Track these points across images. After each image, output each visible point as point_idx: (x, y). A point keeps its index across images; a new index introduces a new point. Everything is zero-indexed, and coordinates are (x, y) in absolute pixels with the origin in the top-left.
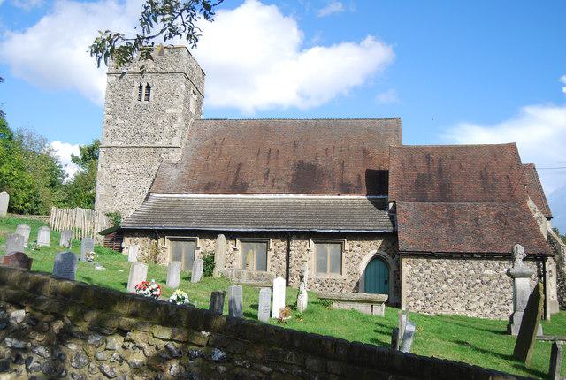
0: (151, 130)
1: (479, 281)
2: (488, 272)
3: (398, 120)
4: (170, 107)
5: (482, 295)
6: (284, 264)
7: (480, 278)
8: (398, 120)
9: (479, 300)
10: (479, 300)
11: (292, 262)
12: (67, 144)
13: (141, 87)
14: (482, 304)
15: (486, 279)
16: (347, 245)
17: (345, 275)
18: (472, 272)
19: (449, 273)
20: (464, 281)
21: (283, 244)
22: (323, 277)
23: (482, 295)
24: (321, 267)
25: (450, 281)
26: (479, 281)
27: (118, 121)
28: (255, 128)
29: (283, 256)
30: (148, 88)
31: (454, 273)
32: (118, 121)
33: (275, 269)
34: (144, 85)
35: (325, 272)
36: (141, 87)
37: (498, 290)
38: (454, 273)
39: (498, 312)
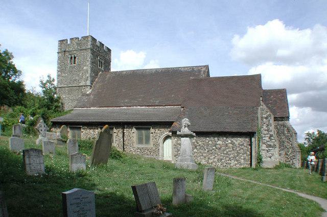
0: (77, 78)
1: (214, 148)
2: (219, 142)
3: (207, 67)
4: (85, 66)
5: (216, 155)
6: (122, 139)
7: (215, 146)
8: (207, 67)
9: (214, 158)
10: (214, 158)
11: (125, 139)
12: (128, 51)
13: (72, 58)
14: (216, 160)
15: (218, 146)
16: (152, 130)
17: (152, 146)
18: (210, 142)
19: (198, 143)
20: (205, 147)
21: (121, 130)
22: (140, 146)
23: (216, 155)
24: (140, 141)
25: (198, 147)
26: (214, 148)
27: (63, 75)
28: (130, 74)
29: (121, 135)
30: (75, 58)
31: (200, 143)
32: (63, 75)
33: (117, 142)
34: (73, 56)
35: (142, 144)
36: (72, 58)
37: (225, 152)
38: (200, 143)
39: (225, 164)
